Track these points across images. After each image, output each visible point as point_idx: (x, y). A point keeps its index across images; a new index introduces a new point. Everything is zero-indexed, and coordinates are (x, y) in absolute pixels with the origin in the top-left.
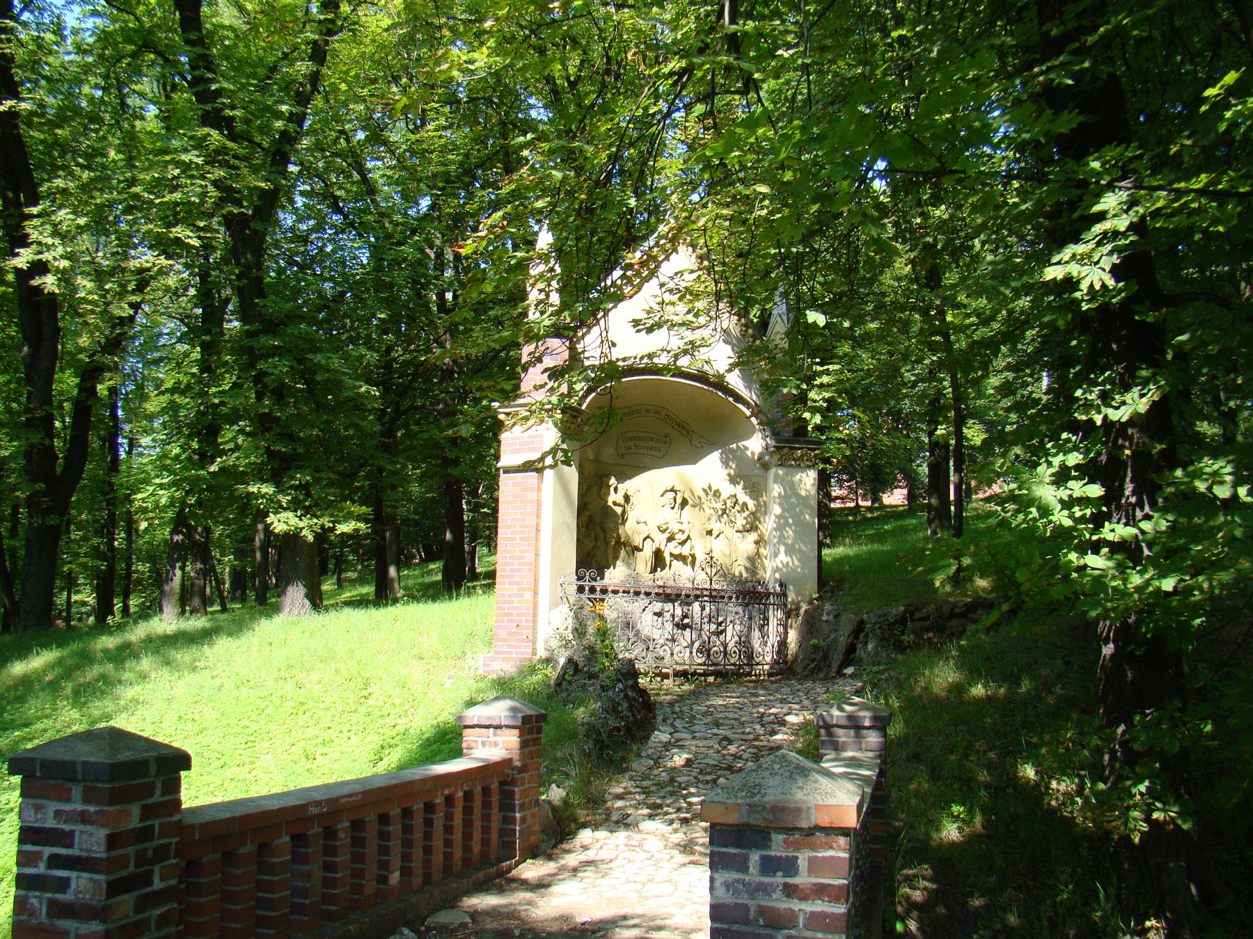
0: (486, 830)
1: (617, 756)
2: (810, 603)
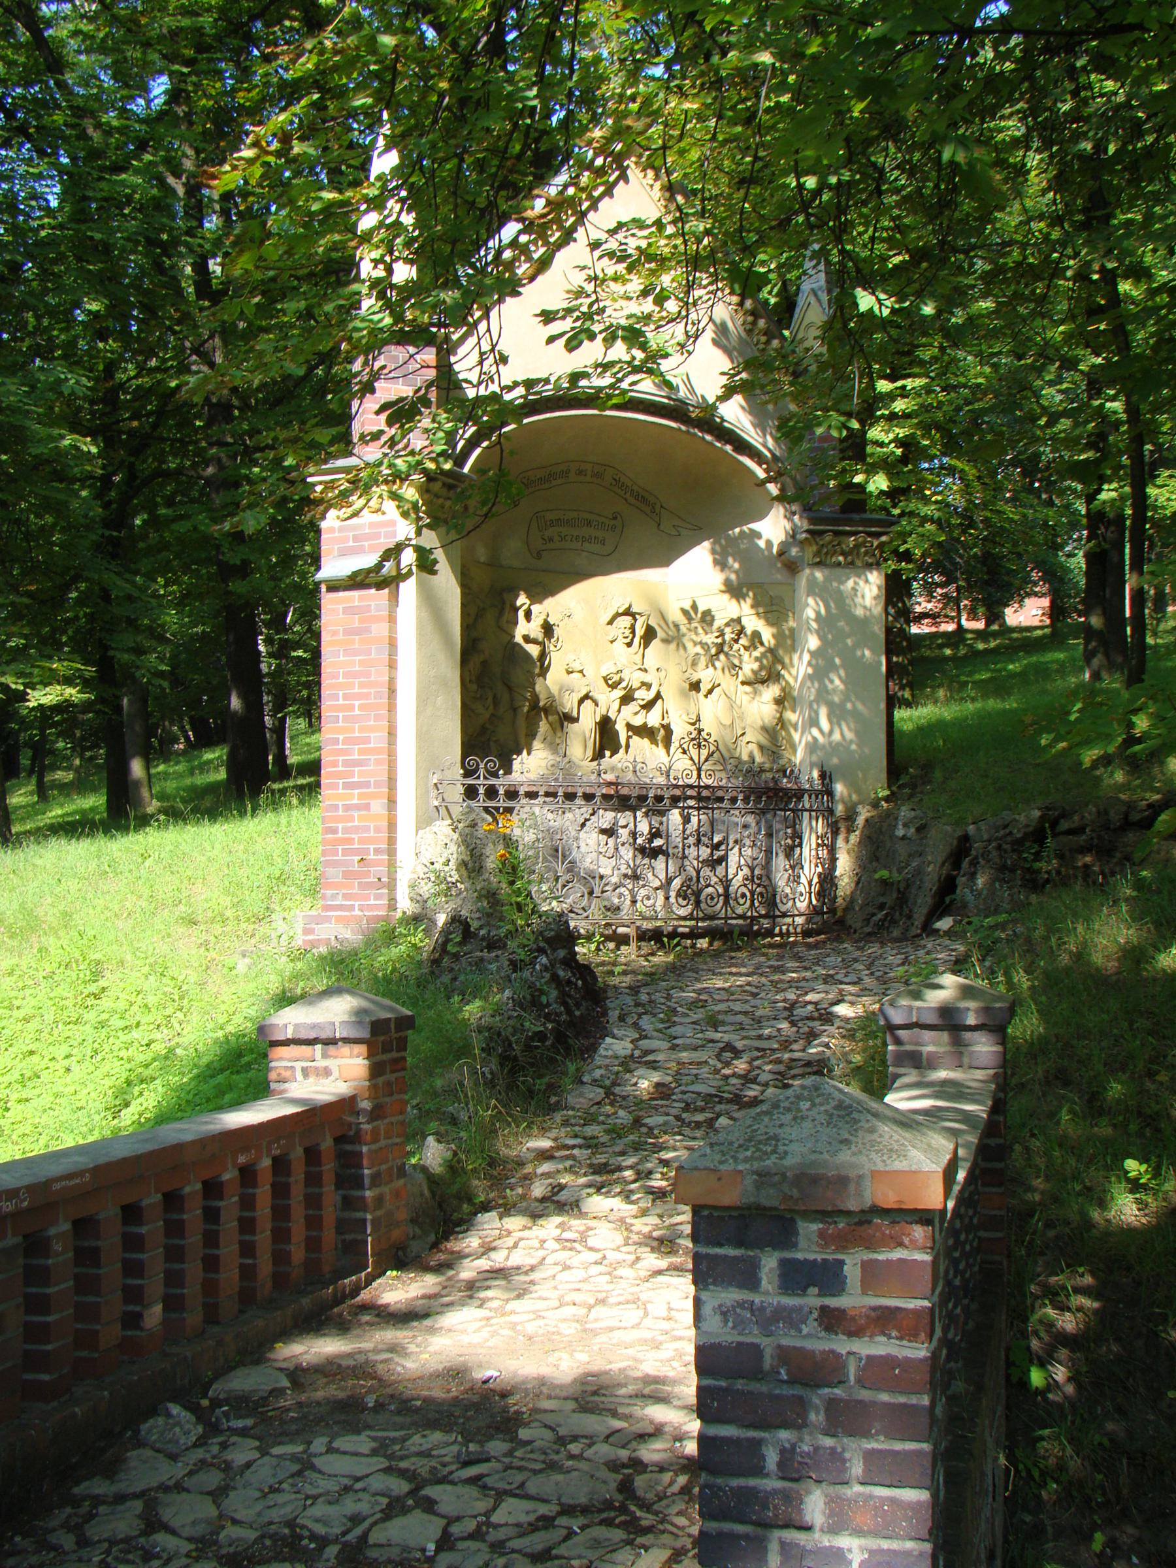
0: (314, 1223)
1: (540, 1084)
2: (875, 805)
